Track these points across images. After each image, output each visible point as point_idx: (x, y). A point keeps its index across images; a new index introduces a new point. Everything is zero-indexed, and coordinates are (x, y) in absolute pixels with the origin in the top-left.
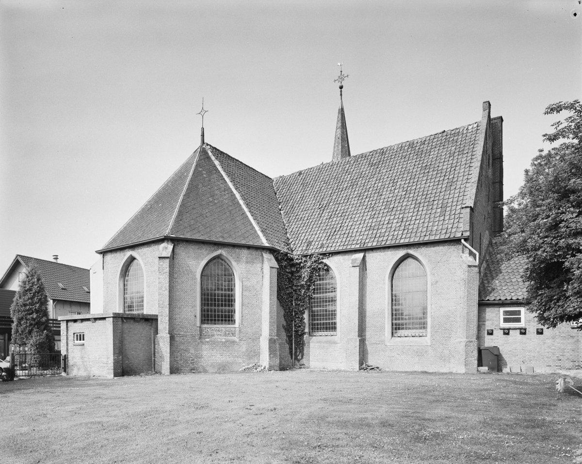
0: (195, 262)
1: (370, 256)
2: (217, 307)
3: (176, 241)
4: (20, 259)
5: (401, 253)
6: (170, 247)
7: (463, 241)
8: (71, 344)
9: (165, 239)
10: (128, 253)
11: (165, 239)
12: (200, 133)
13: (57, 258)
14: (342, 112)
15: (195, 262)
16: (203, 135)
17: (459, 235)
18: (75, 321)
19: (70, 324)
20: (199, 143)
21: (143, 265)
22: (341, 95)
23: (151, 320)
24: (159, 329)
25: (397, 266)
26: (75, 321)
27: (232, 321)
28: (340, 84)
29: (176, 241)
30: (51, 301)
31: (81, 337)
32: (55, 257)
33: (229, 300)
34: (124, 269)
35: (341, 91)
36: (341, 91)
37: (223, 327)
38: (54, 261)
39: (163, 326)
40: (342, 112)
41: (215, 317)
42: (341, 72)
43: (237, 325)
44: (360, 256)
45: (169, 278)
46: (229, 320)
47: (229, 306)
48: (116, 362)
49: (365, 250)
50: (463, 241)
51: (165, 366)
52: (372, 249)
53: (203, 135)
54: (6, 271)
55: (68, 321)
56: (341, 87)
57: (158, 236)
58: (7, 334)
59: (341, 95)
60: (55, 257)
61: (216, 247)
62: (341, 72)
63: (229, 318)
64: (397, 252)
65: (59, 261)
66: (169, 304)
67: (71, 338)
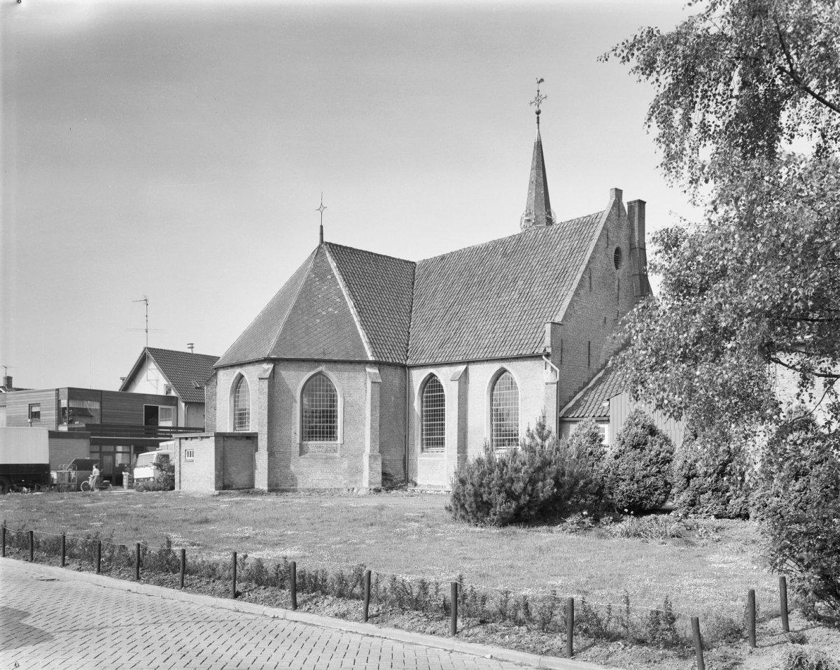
0: (295, 380)
1: (472, 368)
2: (321, 424)
3: (274, 361)
4: (148, 353)
5: (496, 367)
6: (271, 366)
7: (543, 357)
8: (183, 460)
9: (267, 360)
10: (238, 371)
11: (267, 360)
12: (319, 232)
13: (192, 348)
14: (539, 146)
15: (295, 380)
16: (322, 234)
17: (541, 351)
18: (186, 439)
19: (182, 441)
20: (317, 243)
21: (249, 383)
22: (538, 123)
23: (252, 438)
24: (470, 430)
25: (497, 379)
26: (186, 439)
27: (334, 437)
28: (536, 109)
29: (274, 361)
30: (183, 404)
31: (191, 454)
32: (189, 346)
33: (331, 416)
34: (234, 385)
35: (538, 118)
36: (538, 118)
37: (325, 443)
38: (189, 351)
39: (263, 442)
40: (539, 146)
41: (327, 433)
42: (538, 91)
43: (339, 441)
44: (462, 368)
45: (269, 398)
46: (330, 437)
47: (330, 422)
48: (218, 477)
49: (469, 362)
50: (543, 357)
51: (261, 482)
52: (474, 362)
53: (322, 234)
54: (134, 364)
55: (180, 439)
56: (538, 113)
57: (261, 357)
58: (132, 446)
59: (538, 123)
60: (189, 346)
61: (316, 364)
62: (538, 91)
63: (330, 433)
64: (494, 364)
65: (196, 351)
66: (269, 423)
67: (183, 454)
